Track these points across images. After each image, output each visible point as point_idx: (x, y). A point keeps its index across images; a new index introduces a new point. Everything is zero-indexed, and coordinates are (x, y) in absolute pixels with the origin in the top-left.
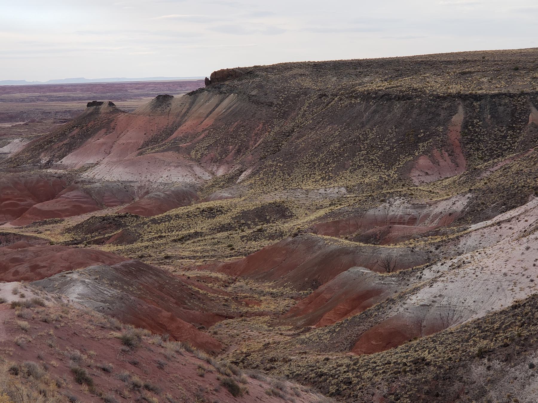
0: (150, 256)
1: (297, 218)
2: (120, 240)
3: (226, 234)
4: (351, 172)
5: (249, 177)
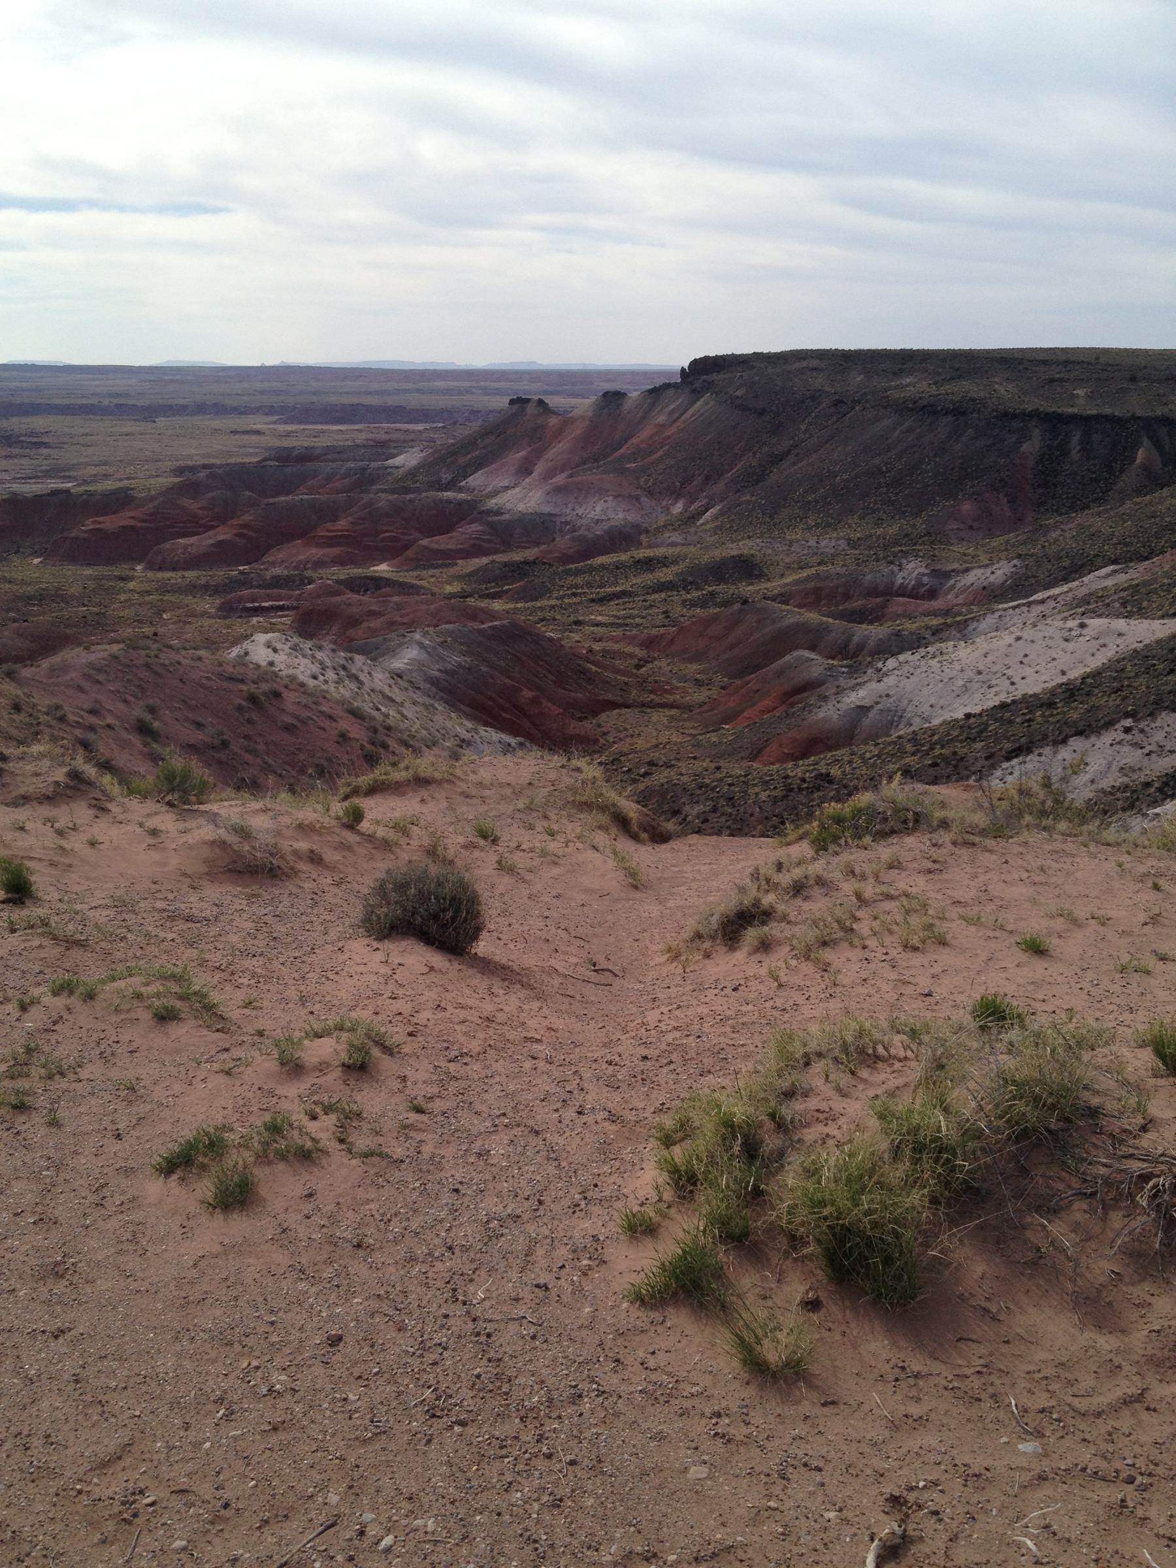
0: (555, 619)
1: (769, 580)
3: (663, 595)
5: (715, 518)
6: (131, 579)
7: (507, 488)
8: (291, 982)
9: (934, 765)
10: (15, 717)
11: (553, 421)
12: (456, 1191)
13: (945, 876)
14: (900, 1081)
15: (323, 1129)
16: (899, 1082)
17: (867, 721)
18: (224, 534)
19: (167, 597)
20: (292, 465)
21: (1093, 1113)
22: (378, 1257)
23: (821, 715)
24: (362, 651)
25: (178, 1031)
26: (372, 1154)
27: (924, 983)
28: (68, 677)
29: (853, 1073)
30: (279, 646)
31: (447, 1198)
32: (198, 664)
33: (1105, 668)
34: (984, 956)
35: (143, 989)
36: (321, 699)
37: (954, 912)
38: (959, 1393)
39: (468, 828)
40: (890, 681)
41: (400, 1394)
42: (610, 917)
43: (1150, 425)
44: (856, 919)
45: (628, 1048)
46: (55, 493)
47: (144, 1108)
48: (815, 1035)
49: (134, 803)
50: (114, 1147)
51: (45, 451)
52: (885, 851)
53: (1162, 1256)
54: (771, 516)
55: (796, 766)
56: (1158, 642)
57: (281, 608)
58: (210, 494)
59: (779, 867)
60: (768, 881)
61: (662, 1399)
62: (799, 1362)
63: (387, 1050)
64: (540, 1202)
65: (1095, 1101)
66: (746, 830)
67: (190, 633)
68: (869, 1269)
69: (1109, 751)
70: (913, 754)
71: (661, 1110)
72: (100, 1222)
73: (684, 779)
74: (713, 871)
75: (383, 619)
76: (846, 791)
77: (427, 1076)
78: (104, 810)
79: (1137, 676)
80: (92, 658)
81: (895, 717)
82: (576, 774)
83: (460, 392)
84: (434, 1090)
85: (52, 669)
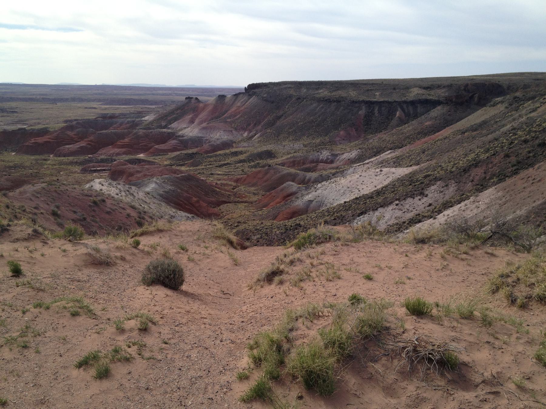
2: (193, 165)
3: (241, 164)
4: (308, 137)
7: (185, 128)
8: (118, 302)
9: (335, 219)
10: (7, 210)
11: (201, 105)
12: (180, 369)
14: (327, 323)
15: (133, 351)
17: (312, 206)
18: (83, 144)
19: (62, 166)
20: (108, 120)
21: (387, 329)
22: (154, 392)
23: (297, 203)
24: (134, 185)
26: (150, 358)
27: (334, 291)
29: (312, 322)
30: (104, 184)
31: (177, 372)
33: (389, 184)
34: (352, 282)
35: (66, 305)
36: (120, 202)
37: (342, 268)
40: (319, 191)
42: (228, 276)
44: (311, 272)
45: (237, 319)
46: (20, 129)
48: (300, 310)
49: (57, 241)
50: (59, 359)
51: (16, 114)
52: (320, 249)
53: (410, 373)
54: (277, 137)
56: (406, 175)
57: (104, 170)
59: (285, 256)
60: (282, 261)
63: (154, 323)
64: (209, 371)
65: (388, 325)
67: (70, 179)
69: (391, 212)
72: (56, 385)
73: (250, 227)
74: (263, 258)
75: (142, 173)
76: (306, 229)
77: (168, 332)
78: (46, 243)
79: (399, 186)
80: (35, 188)
81: (321, 204)
84: (171, 336)
85: (20, 193)
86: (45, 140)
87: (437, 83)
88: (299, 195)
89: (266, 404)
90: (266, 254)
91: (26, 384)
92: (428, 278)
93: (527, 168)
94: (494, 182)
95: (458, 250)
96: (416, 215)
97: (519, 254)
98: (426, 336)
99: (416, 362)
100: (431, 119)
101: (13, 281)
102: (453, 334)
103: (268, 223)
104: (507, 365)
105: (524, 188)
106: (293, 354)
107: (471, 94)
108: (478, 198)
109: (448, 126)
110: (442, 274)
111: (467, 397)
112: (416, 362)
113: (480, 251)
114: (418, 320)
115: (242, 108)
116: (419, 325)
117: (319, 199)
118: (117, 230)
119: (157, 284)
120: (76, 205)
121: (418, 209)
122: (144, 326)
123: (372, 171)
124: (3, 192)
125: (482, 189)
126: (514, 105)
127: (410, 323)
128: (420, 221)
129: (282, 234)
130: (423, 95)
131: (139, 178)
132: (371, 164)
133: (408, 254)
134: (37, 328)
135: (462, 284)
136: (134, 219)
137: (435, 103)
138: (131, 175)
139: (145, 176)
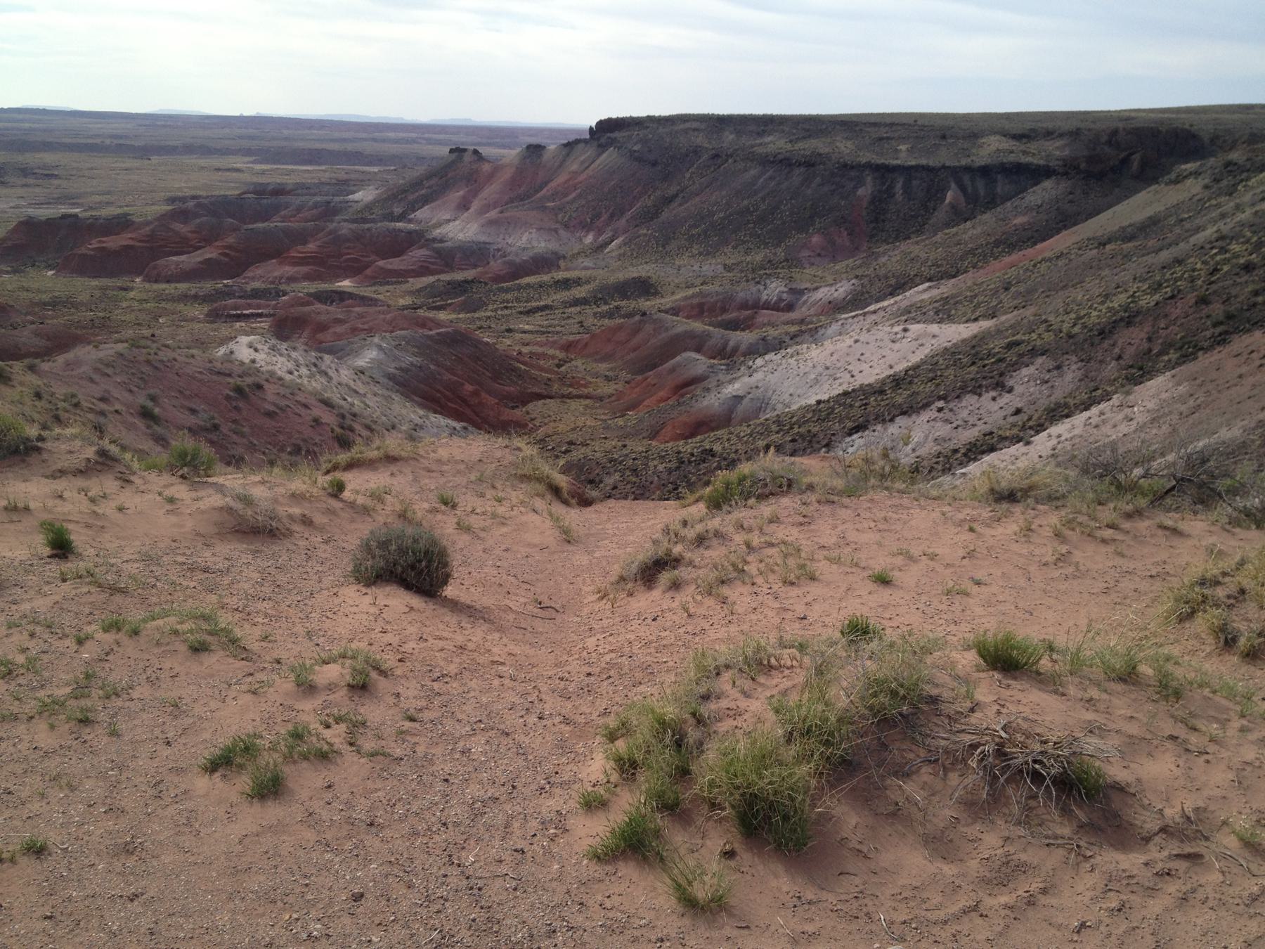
3: (578, 309)
4: (734, 248)
6: (132, 289)
8: (298, 621)
9: (793, 441)
10: (37, 403)
11: (486, 167)
12: (447, 780)
13: (812, 527)
15: (337, 735)
16: (786, 683)
17: (740, 408)
18: (210, 253)
19: (163, 304)
20: (269, 198)
21: (934, 700)
22: (387, 833)
23: (705, 403)
24: (330, 351)
25: (210, 660)
27: (800, 609)
28: (81, 371)
29: (753, 679)
30: (259, 347)
31: (439, 786)
32: (191, 360)
33: (923, 362)
34: (844, 589)
37: (820, 555)
38: (841, 914)
39: (431, 496)
40: (758, 376)
41: (412, 935)
43: (956, 172)
44: (746, 562)
45: (574, 666)
46: (64, 217)
47: (187, 721)
48: (724, 652)
49: (152, 476)
50: (167, 751)
51: (56, 182)
52: (766, 509)
54: (664, 246)
55: (686, 443)
56: (963, 341)
57: (260, 315)
58: (198, 221)
59: (685, 523)
61: (618, 931)
62: (721, 897)
63: (383, 673)
64: (514, 787)
65: (935, 692)
66: (647, 494)
67: (182, 335)
68: (769, 824)
69: (926, 426)
70: (777, 432)
71: (605, 713)
73: (597, 455)
74: (634, 528)
75: (346, 326)
77: (416, 693)
79: (947, 367)
80: (101, 354)
81: (762, 405)
82: (517, 452)
83: (407, 141)
84: (423, 703)
85: (68, 364)
86: (125, 243)
87: (1045, 125)
88: (711, 383)
89: (649, 865)
90: (638, 519)
91: (90, 806)
92: (1022, 582)
93: (1249, 331)
94: (1170, 360)
95: (1095, 519)
96: (985, 435)
97: (1237, 530)
98: (1025, 719)
99: (1002, 780)
100: (1029, 209)
101: (53, 567)
102: (1090, 716)
103: (638, 446)
104: (1218, 792)
105: (1240, 376)
106: (711, 755)
107: (1123, 155)
108: (1131, 397)
109: (1066, 227)
110: (1056, 574)
111: (1125, 865)
112: (1002, 780)
113: (1147, 523)
114: (1005, 682)
115: (581, 178)
116: (1009, 693)
117: (758, 393)
118: (290, 453)
119: (387, 581)
120: (196, 395)
121: (990, 420)
122: (360, 679)
123: (884, 331)
124: (27, 361)
125: (1141, 376)
126: (1225, 183)
127: (988, 688)
128: (992, 449)
129: (670, 471)
130: (1012, 152)
131: (339, 337)
132: (882, 313)
133: (975, 526)
134: (110, 679)
135: (1104, 598)
136: (328, 429)
137: (1037, 174)
138: (322, 327)
139: (354, 330)
